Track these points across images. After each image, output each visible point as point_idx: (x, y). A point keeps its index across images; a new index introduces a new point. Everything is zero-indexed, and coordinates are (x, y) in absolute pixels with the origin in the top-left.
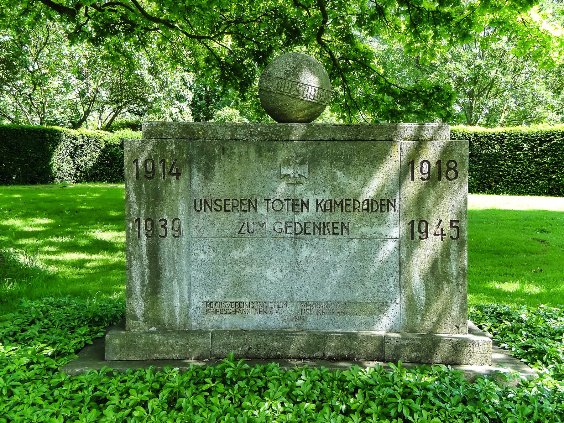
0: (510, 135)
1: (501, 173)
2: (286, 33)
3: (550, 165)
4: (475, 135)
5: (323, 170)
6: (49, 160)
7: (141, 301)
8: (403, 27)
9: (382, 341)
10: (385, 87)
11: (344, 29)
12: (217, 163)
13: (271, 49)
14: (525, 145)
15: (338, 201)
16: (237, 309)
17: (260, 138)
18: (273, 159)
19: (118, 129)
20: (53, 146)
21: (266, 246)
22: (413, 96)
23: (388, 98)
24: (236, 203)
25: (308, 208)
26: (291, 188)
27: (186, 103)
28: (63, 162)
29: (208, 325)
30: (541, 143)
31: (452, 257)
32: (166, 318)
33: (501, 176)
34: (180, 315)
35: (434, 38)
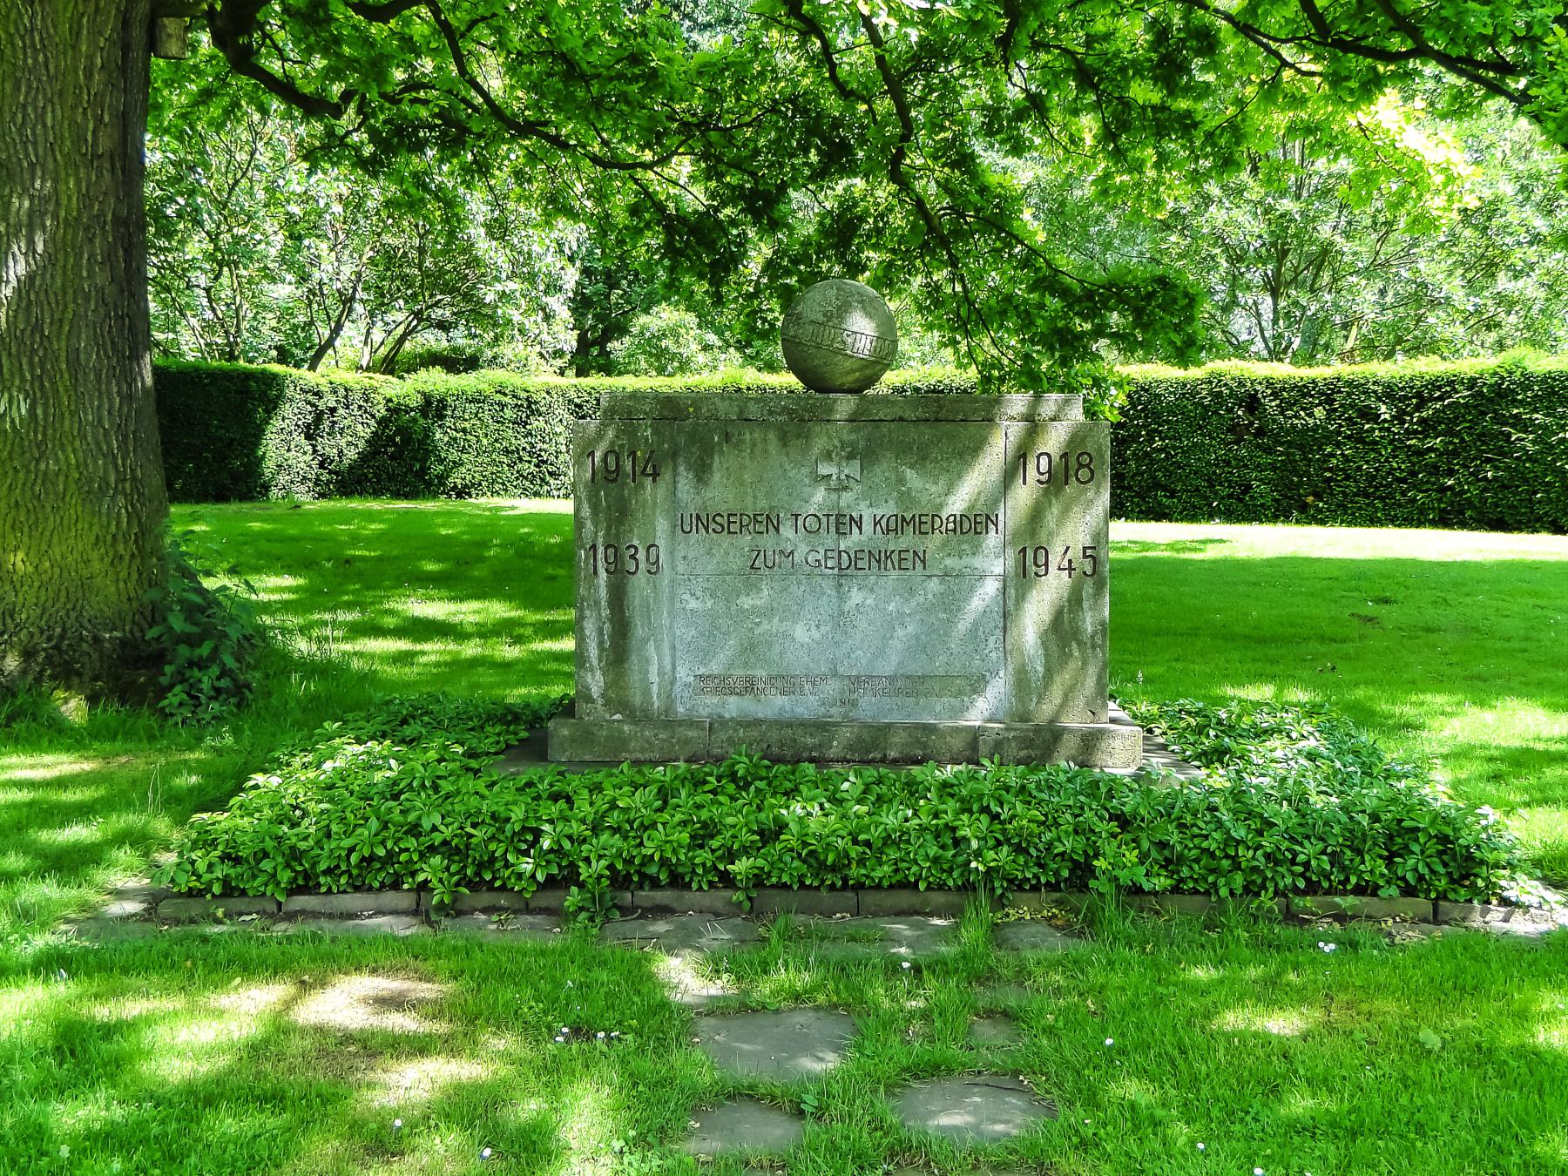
0: (1350, 383)
1: (1328, 475)
2: (818, 149)
3: (1442, 454)
4: (1269, 383)
5: (883, 470)
6: (257, 444)
7: (598, 673)
8: (1089, 140)
9: (975, 735)
10: (1045, 277)
11: (954, 139)
12: (716, 458)
13: (782, 188)
14: (1383, 408)
15: (908, 516)
16: (749, 687)
17: (784, 418)
18: (805, 451)
19: (411, 369)
20: (267, 411)
21: (793, 588)
22: (1110, 298)
23: (1054, 303)
24: (745, 520)
25: (860, 528)
26: (834, 496)
27: (561, 297)
28: (289, 450)
29: (704, 712)
30: (1422, 403)
31: (1086, 605)
32: (637, 700)
33: (1329, 480)
34: (659, 695)
35: (1157, 166)
